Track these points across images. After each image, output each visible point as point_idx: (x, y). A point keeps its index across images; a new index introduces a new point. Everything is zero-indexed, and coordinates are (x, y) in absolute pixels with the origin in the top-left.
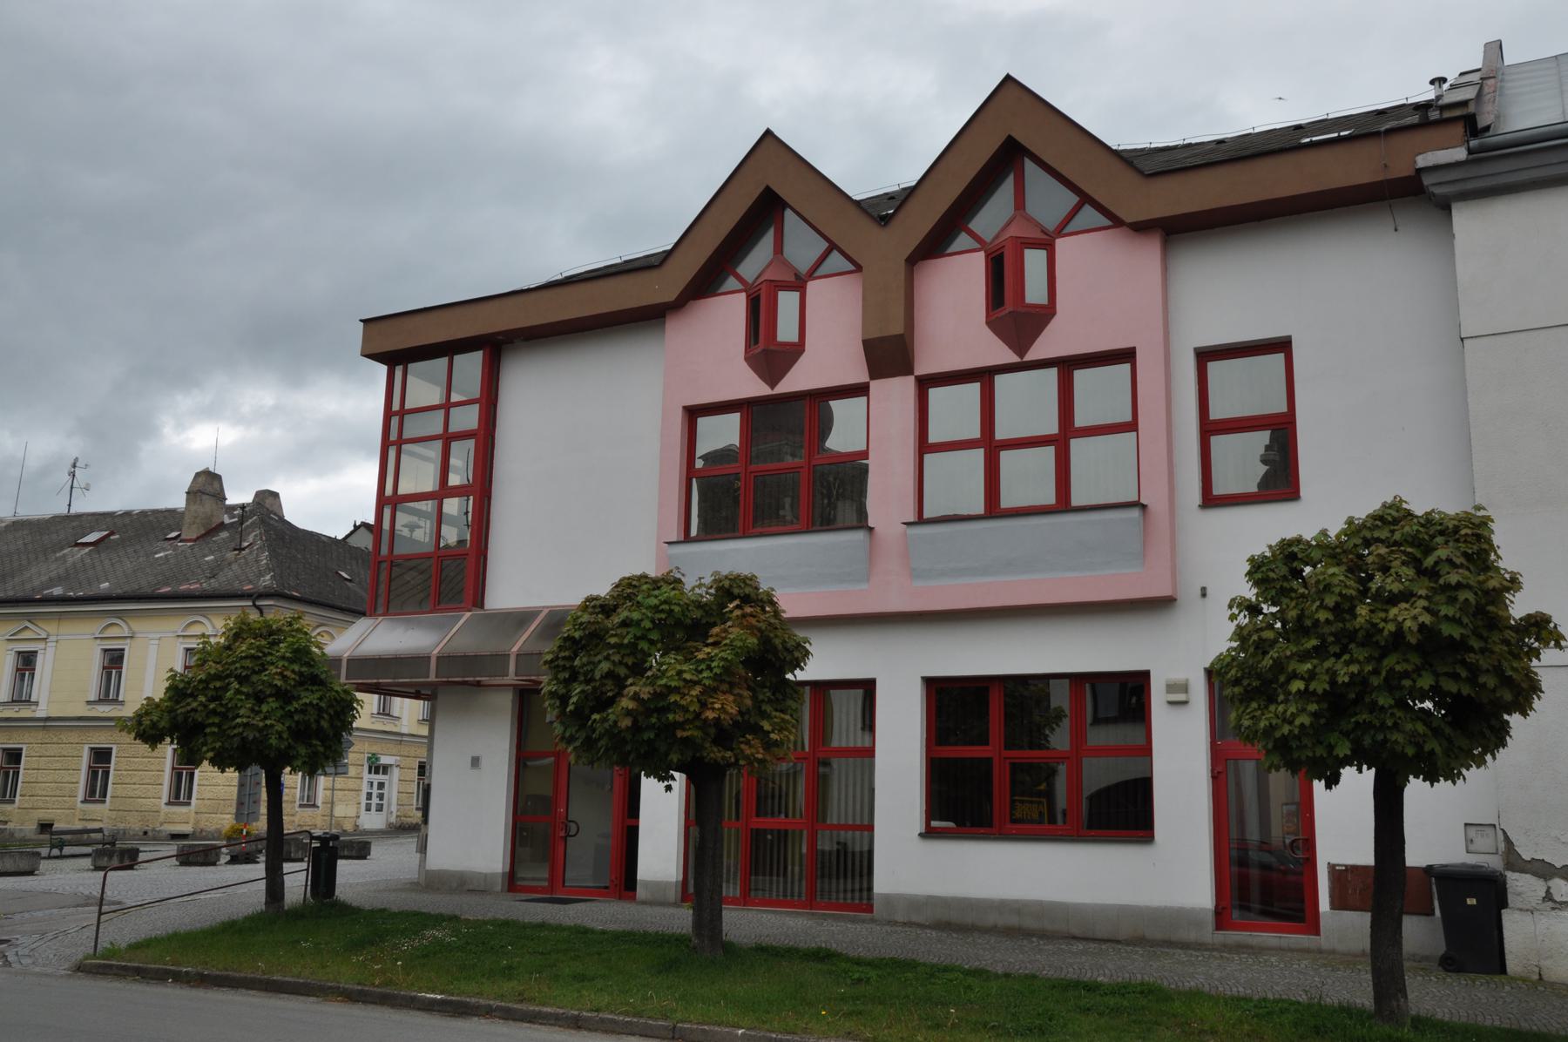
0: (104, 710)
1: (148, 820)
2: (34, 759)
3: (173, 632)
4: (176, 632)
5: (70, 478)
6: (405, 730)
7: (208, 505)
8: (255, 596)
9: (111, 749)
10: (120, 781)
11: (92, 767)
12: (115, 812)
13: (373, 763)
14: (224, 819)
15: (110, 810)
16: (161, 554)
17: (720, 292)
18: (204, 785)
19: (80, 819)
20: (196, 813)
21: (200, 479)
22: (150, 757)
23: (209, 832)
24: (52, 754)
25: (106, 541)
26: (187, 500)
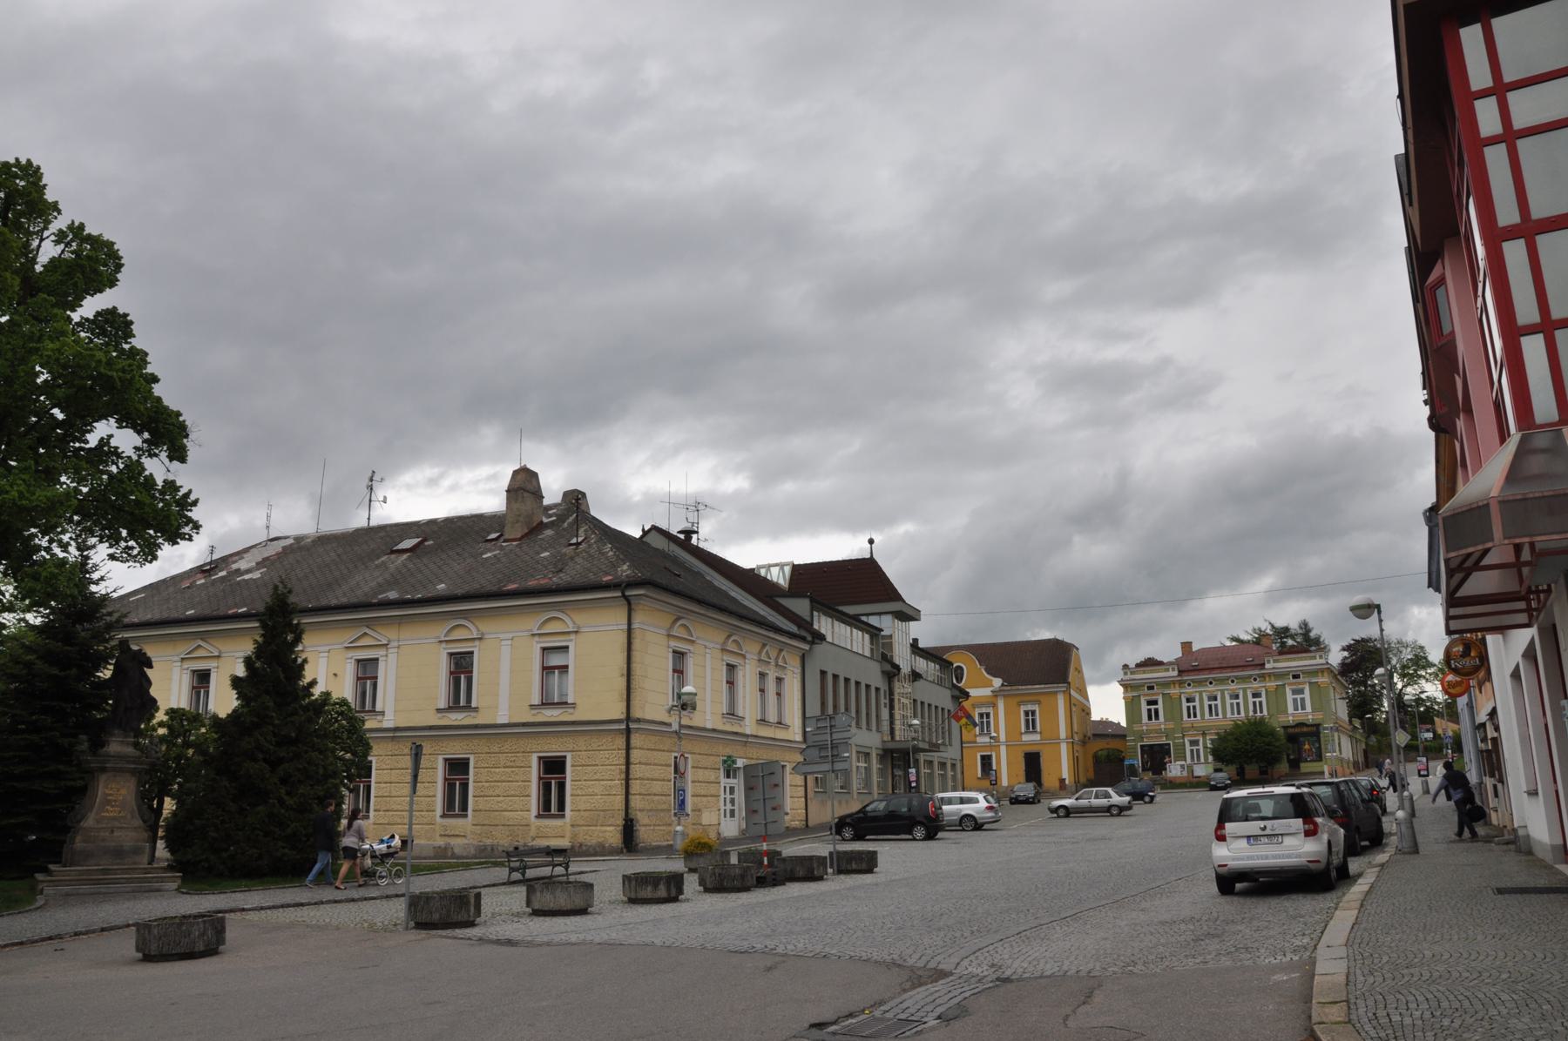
0: (456, 718)
1: (518, 835)
2: (385, 771)
3: (528, 631)
4: (531, 630)
5: (368, 491)
6: (748, 732)
7: (527, 505)
8: (623, 585)
9: (565, 757)
10: (482, 794)
11: (543, 778)
12: (479, 827)
13: (729, 766)
14: (606, 831)
15: (474, 825)
16: (489, 555)
17: (215, 644)
18: (578, 795)
19: (441, 835)
20: (572, 826)
21: (519, 477)
22: (512, 767)
23: (591, 846)
24: (404, 767)
25: (422, 546)
26: (508, 499)
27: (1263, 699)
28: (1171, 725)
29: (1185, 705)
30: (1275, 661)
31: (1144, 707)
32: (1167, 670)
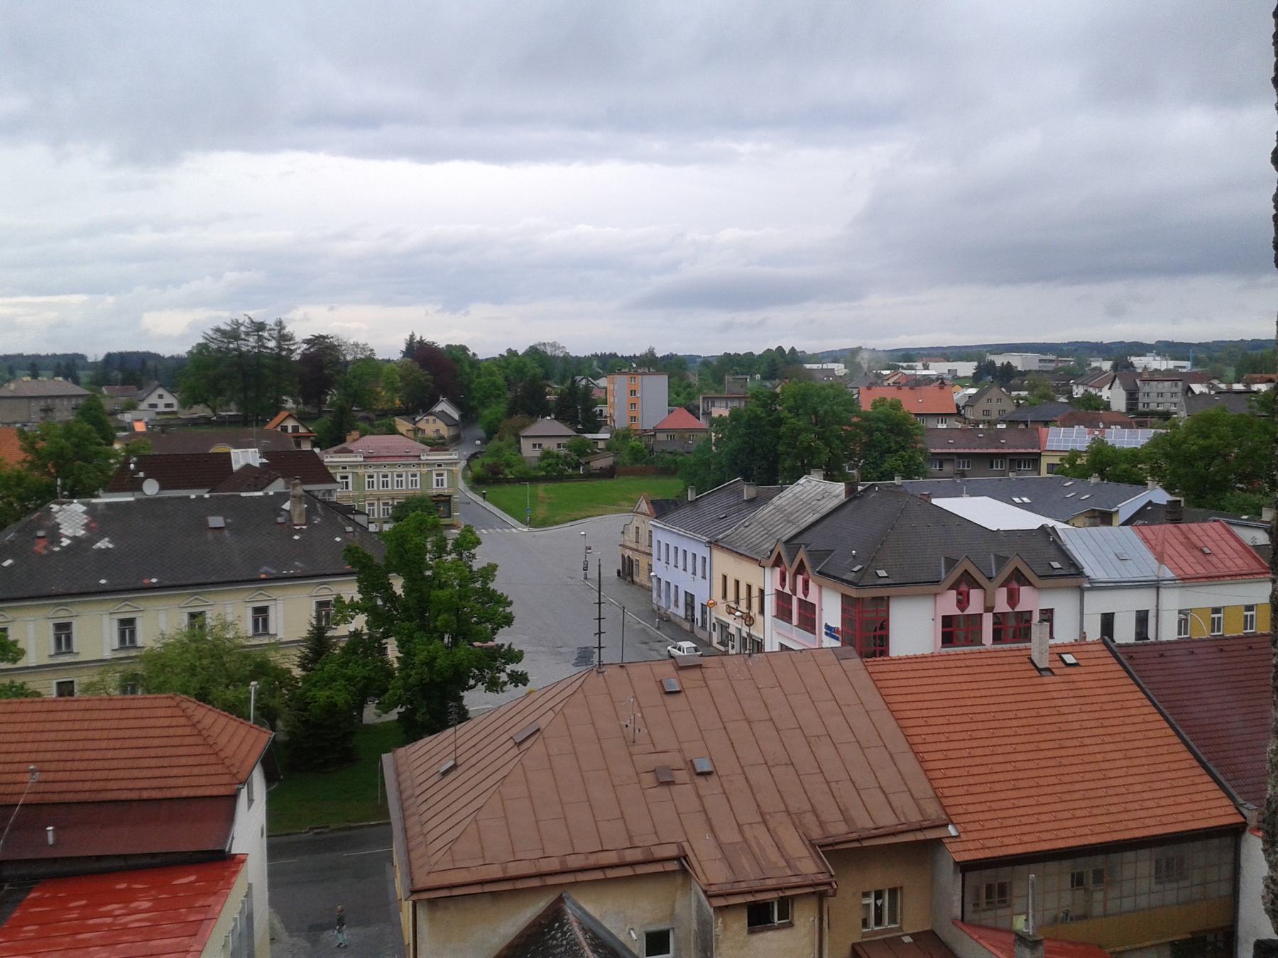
27: (418, 478)
29: (367, 480)
30: (331, 457)
31: (435, 478)
32: (356, 457)
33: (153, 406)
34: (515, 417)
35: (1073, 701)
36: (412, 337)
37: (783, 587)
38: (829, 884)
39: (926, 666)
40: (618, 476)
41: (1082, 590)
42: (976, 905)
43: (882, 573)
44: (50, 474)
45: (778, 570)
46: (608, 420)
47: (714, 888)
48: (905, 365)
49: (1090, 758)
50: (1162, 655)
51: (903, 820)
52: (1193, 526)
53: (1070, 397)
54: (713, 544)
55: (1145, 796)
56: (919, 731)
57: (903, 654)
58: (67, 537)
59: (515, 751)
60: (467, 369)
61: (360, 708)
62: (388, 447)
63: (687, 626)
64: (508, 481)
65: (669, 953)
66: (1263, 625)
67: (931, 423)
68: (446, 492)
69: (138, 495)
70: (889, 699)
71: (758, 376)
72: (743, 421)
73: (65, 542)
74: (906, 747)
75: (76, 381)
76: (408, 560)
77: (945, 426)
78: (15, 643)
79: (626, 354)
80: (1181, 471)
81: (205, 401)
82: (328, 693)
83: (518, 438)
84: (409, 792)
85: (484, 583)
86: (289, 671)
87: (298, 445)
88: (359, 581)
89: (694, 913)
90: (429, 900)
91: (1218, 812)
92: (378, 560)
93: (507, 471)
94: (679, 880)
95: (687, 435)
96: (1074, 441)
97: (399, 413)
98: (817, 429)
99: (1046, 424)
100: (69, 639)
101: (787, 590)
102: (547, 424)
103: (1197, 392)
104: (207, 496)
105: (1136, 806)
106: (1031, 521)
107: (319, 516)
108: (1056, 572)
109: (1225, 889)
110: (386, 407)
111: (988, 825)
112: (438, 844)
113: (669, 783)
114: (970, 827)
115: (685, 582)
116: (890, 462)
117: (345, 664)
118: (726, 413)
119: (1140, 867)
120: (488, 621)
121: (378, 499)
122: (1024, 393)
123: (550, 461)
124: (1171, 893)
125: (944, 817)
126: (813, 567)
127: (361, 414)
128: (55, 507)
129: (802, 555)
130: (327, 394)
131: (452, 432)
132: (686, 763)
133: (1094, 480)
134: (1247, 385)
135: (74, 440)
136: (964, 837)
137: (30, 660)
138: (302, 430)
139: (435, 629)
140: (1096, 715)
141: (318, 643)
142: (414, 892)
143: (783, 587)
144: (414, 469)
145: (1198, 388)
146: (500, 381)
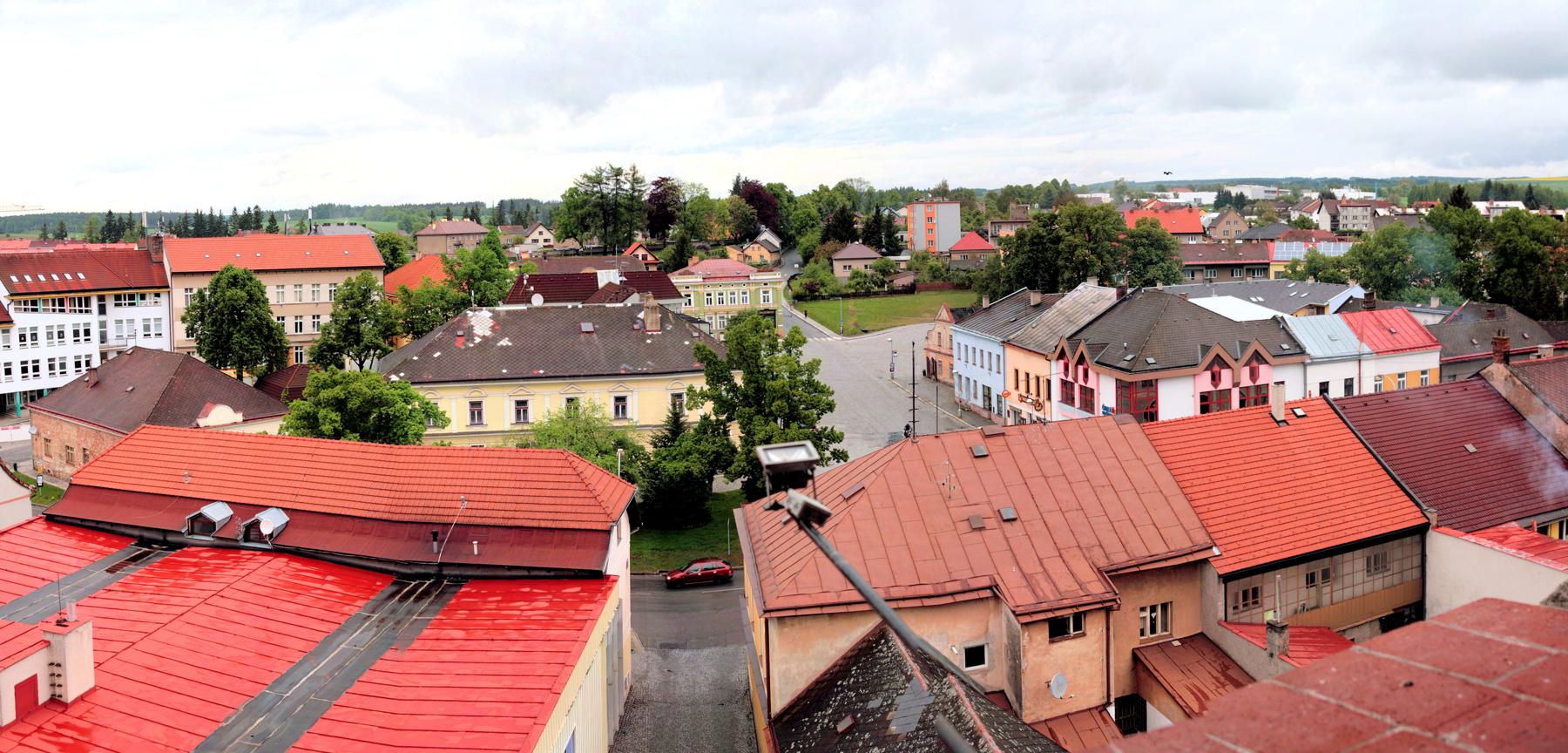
27: (748, 295)
28: (697, 309)
31: (762, 295)
33: (535, 241)
34: (828, 243)
35: (1303, 444)
36: (738, 177)
37: (1067, 376)
38: (1115, 600)
39: (1191, 425)
40: (919, 292)
41: (1304, 365)
42: (1235, 608)
43: (1151, 360)
44: (464, 291)
45: (1062, 362)
46: (909, 244)
47: (1020, 608)
48: (1159, 194)
49: (1317, 486)
50: (1366, 405)
51: (1172, 549)
52: (1382, 312)
53: (1289, 221)
54: (1006, 343)
55: (1358, 510)
56: (1188, 477)
57: (1172, 417)
58: (479, 336)
59: (845, 505)
60: (786, 203)
61: (710, 477)
62: (723, 270)
63: (985, 414)
64: (823, 298)
65: (983, 663)
66: (1433, 380)
67: (1184, 240)
68: (771, 307)
69: (529, 305)
70: (1194, 504)
71: (1037, 205)
72: (1027, 239)
73: (478, 340)
74: (1178, 491)
75: (479, 222)
76: (745, 356)
77: (1194, 242)
78: (443, 413)
79: (922, 189)
80: (1373, 273)
81: (574, 236)
82: (685, 464)
83: (831, 260)
84: (757, 537)
85: (810, 375)
86: (642, 448)
87: (647, 268)
88: (708, 375)
89: (1004, 631)
90: (780, 619)
91: (1412, 518)
92: (722, 357)
93: (822, 290)
94: (992, 603)
95: (978, 256)
96: (1295, 253)
97: (729, 243)
98: (1091, 245)
99: (1272, 240)
100: (480, 414)
101: (1070, 379)
102: (856, 249)
103: (1381, 214)
104: (580, 306)
105: (1352, 518)
106: (1267, 314)
107: (671, 323)
108: (1286, 352)
109: (1416, 573)
110: (718, 238)
111: (1243, 544)
112: (784, 576)
113: (981, 529)
114: (1229, 547)
115: (983, 377)
116: (1152, 272)
117: (698, 442)
118: (1012, 234)
119: (1355, 565)
120: (814, 407)
121: (716, 314)
122: (1254, 218)
123: (859, 280)
124: (1378, 582)
125: (1209, 541)
126: (1092, 358)
127: (697, 245)
128: (470, 313)
129: (1082, 348)
130: (669, 228)
131: (775, 257)
132: (994, 512)
133: (1311, 281)
134: (1417, 210)
135: (482, 263)
136: (1225, 555)
137: (452, 428)
138: (650, 258)
139: (771, 413)
140: (1320, 453)
141: (676, 425)
142: (765, 612)
143: (1067, 376)
144: (744, 288)
145: (1382, 212)
146: (814, 212)
